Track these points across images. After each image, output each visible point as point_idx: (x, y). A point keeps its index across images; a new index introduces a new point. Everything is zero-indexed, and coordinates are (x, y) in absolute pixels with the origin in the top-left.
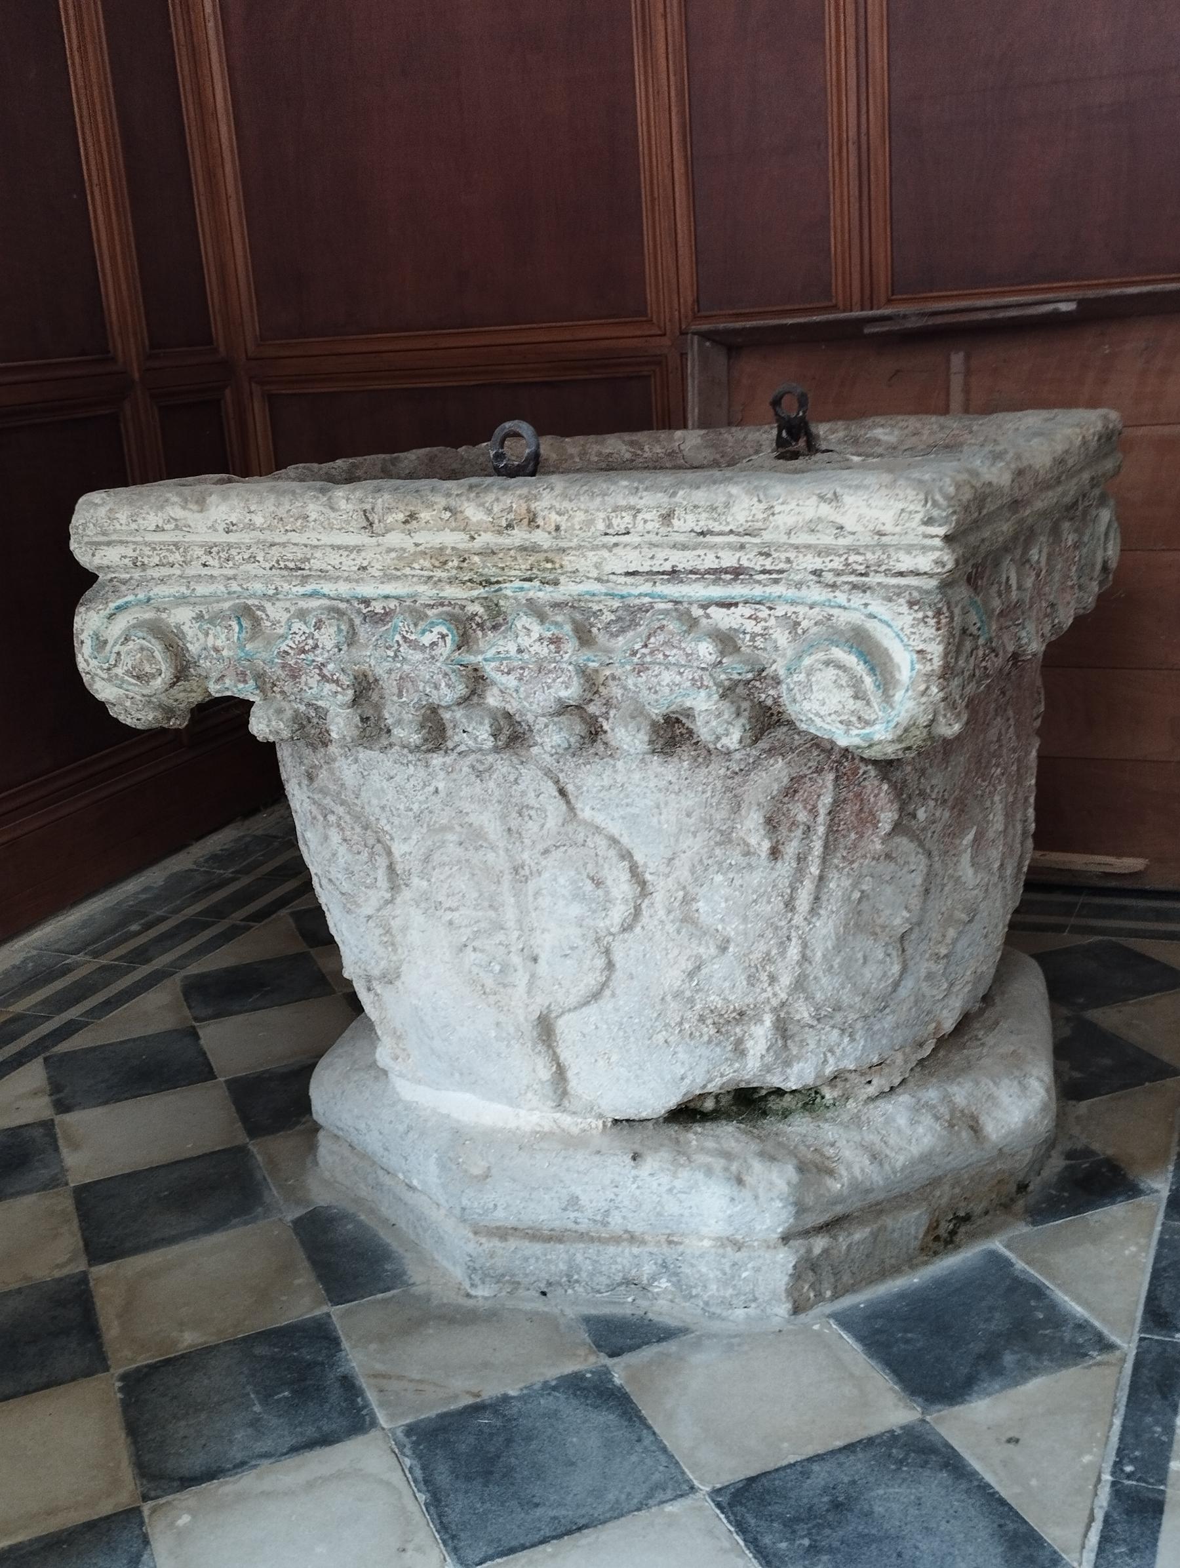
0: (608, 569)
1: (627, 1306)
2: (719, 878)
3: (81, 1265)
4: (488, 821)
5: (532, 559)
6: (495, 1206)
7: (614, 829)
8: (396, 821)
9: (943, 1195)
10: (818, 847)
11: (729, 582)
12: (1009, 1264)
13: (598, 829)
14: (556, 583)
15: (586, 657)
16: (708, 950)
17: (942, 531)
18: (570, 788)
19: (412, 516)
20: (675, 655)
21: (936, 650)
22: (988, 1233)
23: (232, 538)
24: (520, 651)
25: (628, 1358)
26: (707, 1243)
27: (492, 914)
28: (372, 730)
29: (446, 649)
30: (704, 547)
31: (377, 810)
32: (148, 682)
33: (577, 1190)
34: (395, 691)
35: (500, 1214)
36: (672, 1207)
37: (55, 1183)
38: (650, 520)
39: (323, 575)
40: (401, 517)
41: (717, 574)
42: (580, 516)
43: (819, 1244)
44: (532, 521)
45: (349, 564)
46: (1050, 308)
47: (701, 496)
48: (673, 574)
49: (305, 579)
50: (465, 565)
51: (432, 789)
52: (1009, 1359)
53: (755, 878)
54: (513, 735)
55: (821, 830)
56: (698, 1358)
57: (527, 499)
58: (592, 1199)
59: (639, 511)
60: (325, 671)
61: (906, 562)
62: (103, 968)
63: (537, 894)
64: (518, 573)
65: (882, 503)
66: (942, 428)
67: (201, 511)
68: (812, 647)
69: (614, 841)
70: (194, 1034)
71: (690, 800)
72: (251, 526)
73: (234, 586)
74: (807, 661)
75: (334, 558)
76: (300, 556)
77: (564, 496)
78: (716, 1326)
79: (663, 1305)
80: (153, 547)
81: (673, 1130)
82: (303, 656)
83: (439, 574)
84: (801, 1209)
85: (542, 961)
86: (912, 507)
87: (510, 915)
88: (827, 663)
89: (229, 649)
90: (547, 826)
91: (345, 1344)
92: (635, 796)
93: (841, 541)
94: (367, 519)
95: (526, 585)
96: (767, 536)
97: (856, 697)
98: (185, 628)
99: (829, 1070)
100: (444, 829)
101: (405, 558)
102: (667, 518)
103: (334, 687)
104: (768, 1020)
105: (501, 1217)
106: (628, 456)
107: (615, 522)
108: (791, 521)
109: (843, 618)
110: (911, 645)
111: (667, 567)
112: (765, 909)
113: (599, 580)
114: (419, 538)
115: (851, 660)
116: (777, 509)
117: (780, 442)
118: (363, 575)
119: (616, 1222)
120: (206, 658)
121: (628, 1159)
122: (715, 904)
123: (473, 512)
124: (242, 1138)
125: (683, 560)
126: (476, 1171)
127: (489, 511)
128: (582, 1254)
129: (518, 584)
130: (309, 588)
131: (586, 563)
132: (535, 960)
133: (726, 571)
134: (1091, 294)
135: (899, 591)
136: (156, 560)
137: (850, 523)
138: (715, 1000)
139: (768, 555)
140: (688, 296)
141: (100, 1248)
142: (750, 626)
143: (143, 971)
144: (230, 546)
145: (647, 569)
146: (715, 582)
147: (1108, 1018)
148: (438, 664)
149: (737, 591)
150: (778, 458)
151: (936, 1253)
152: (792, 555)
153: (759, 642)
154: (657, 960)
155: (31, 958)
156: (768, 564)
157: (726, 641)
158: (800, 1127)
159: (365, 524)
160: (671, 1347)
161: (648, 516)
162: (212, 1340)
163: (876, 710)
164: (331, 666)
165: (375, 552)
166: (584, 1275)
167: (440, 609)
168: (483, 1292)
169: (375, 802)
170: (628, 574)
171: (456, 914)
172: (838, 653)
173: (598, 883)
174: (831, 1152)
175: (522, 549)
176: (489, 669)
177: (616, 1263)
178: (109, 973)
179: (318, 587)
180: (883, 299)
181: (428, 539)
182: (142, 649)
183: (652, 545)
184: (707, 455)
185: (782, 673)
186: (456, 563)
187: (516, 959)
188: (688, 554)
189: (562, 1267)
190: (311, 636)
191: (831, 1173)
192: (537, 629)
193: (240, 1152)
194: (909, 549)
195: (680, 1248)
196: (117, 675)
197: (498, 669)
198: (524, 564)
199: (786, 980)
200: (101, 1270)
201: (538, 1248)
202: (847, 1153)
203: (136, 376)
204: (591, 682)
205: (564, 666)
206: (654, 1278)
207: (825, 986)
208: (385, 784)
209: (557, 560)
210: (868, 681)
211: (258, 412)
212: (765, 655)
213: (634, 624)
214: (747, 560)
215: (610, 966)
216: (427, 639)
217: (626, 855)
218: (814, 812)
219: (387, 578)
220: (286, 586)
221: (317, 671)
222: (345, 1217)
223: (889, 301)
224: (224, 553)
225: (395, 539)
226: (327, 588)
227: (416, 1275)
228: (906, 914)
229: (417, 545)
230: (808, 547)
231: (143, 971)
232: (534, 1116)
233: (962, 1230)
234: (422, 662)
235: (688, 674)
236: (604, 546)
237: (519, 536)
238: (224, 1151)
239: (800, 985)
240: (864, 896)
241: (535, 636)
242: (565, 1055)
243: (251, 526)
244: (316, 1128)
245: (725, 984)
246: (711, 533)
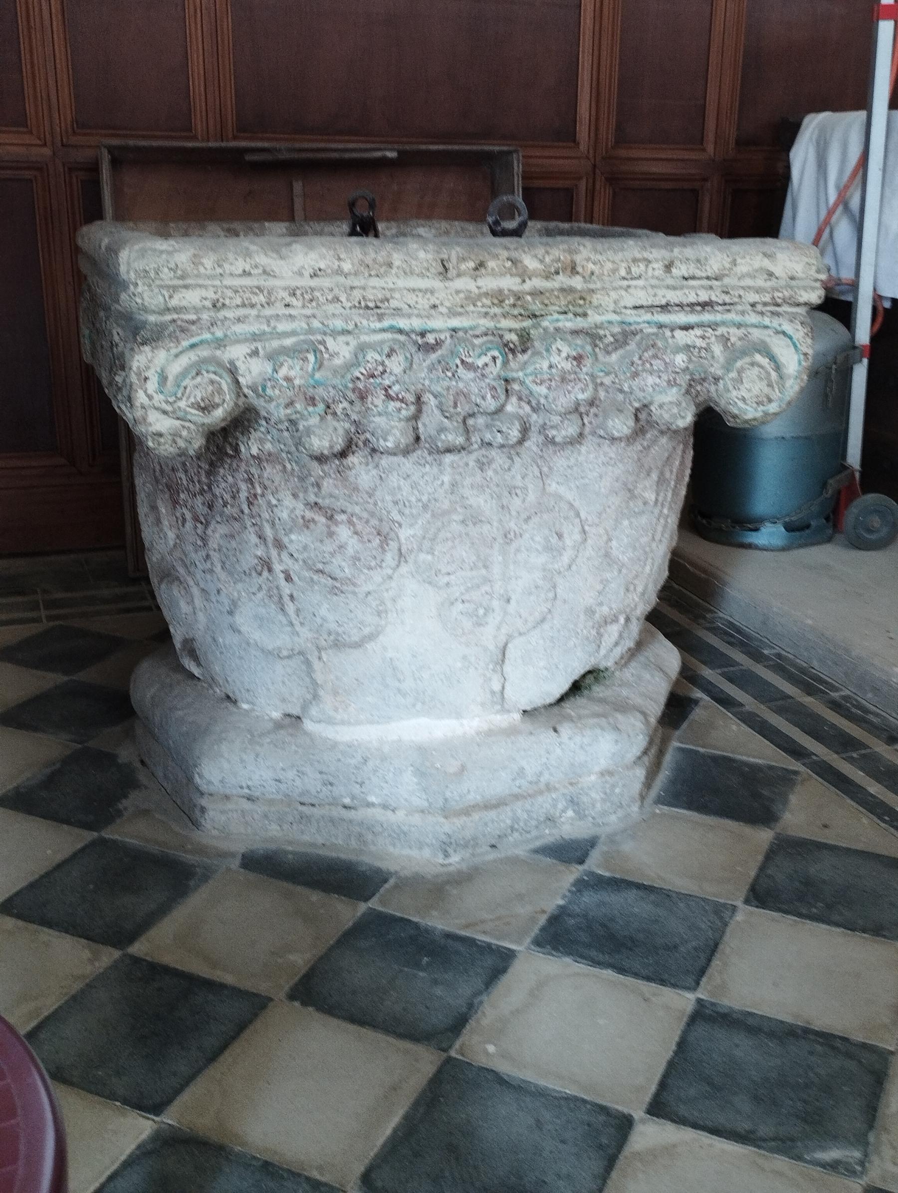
0: (622, 304)
4: (482, 502)
5: (570, 298)
6: (469, 791)
8: (407, 511)
11: (699, 312)
12: (697, 752)
14: (585, 315)
23: (314, 283)
24: (551, 367)
26: (593, 778)
27: (484, 571)
31: (390, 505)
32: (209, 412)
33: (524, 763)
34: (452, 404)
35: (471, 797)
40: (471, 265)
42: (609, 266)
45: (424, 303)
46: (378, 154)
47: (689, 252)
48: (665, 308)
49: (380, 317)
50: (519, 303)
51: (439, 482)
57: (570, 252)
58: (531, 768)
59: (650, 262)
60: (390, 392)
63: (518, 550)
64: (557, 308)
65: (797, 259)
68: (744, 353)
72: (339, 272)
73: (316, 324)
74: (739, 364)
75: (411, 299)
76: (380, 296)
81: (556, 710)
82: (372, 380)
83: (496, 310)
85: (513, 602)
87: (496, 570)
88: (753, 364)
89: (301, 377)
90: (529, 499)
94: (444, 266)
95: (562, 317)
97: (768, 385)
98: (239, 364)
100: (445, 513)
101: (472, 299)
102: (668, 267)
103: (398, 404)
105: (473, 797)
107: (633, 269)
111: (663, 302)
113: (615, 312)
114: (480, 282)
116: (739, 261)
118: (433, 312)
120: (273, 387)
125: (674, 297)
126: (452, 770)
127: (542, 261)
128: (519, 809)
129: (556, 316)
130: (386, 323)
132: (508, 601)
133: (699, 304)
134: (407, 147)
136: (238, 301)
137: (778, 270)
139: (727, 293)
144: (312, 290)
145: (650, 303)
146: (692, 311)
148: (487, 381)
149: (707, 317)
152: (742, 293)
156: (727, 299)
159: (441, 269)
161: (656, 266)
164: (396, 388)
165: (446, 292)
166: (522, 824)
167: (485, 338)
168: (455, 859)
169: (388, 498)
170: (636, 308)
171: (452, 577)
175: (562, 290)
177: (542, 807)
179: (394, 323)
180: (230, 136)
181: (488, 283)
182: (212, 382)
186: (512, 301)
187: (495, 604)
188: (679, 293)
189: (509, 822)
190: (383, 364)
192: (566, 350)
194: (805, 288)
195: (579, 786)
196: (179, 408)
197: (534, 382)
201: (492, 814)
205: (582, 376)
208: (402, 482)
209: (588, 298)
212: (706, 362)
214: (716, 296)
216: (480, 363)
219: (452, 313)
220: (365, 322)
221: (383, 392)
223: (235, 138)
224: (310, 297)
225: (465, 284)
226: (403, 323)
229: (478, 288)
230: (749, 287)
234: (474, 380)
235: (665, 377)
236: (621, 288)
237: (562, 280)
241: (564, 355)
243: (339, 272)
246: (693, 278)
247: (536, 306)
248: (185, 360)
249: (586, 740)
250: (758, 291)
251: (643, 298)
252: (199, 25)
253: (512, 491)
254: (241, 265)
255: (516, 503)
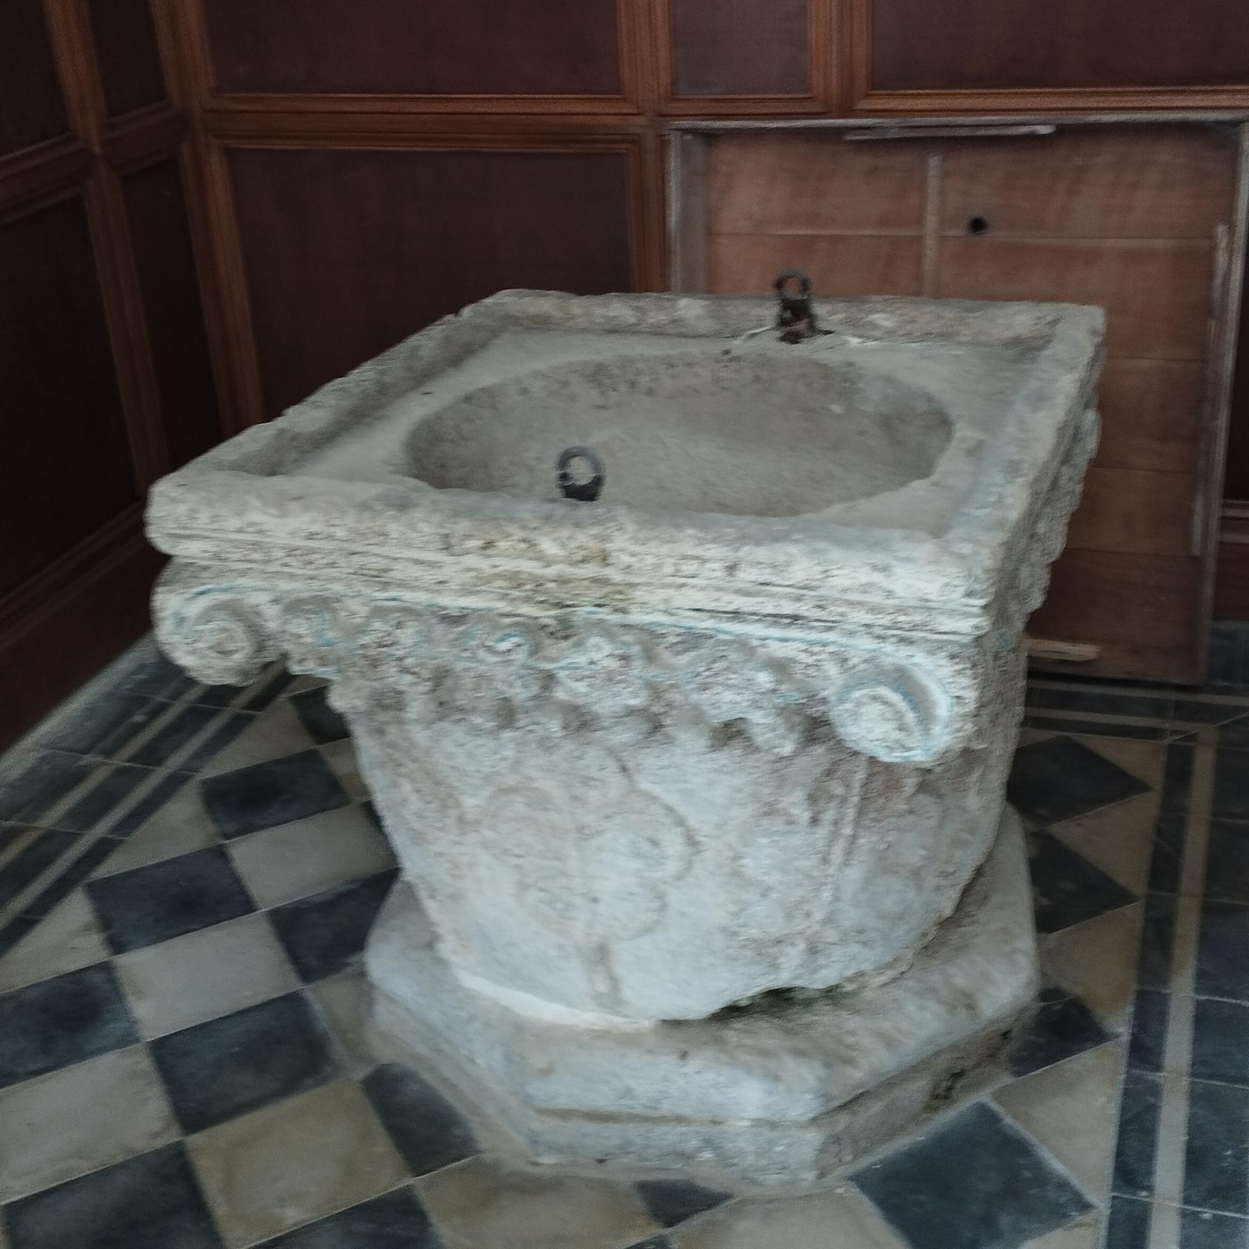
0: (675, 604)
1: (675, 1173)
2: (764, 841)
3: (173, 1136)
5: (605, 590)
7: (670, 799)
9: (942, 1064)
10: (851, 813)
13: (654, 799)
15: (652, 672)
16: (749, 895)
17: (982, 602)
18: (630, 765)
19: (489, 545)
20: (735, 679)
21: (971, 695)
22: (978, 1085)
25: (682, 1227)
28: (444, 708)
29: (520, 656)
30: (768, 596)
33: (631, 1083)
36: (716, 1098)
37: (128, 1039)
38: (715, 570)
39: (402, 584)
40: (480, 543)
41: (776, 619)
42: (650, 560)
43: (843, 1121)
44: (604, 558)
48: (736, 615)
49: (386, 585)
52: (1005, 1220)
53: (796, 841)
54: (581, 721)
55: (856, 800)
56: (743, 1226)
61: (948, 624)
62: (120, 772)
66: (940, 317)
67: (280, 517)
68: (860, 683)
69: (670, 810)
70: (221, 854)
71: (740, 780)
74: (857, 694)
75: (415, 571)
77: (635, 540)
78: (755, 1191)
79: (705, 1172)
80: (236, 544)
81: (714, 1028)
83: (515, 593)
84: (826, 1097)
86: (956, 582)
88: (875, 698)
91: (434, 1218)
92: (691, 777)
93: (891, 602)
96: (822, 592)
97: (901, 729)
99: (850, 972)
102: (732, 569)
104: (802, 946)
105: (563, 1102)
106: (632, 320)
108: (846, 583)
109: (887, 661)
110: (951, 692)
111: (731, 608)
112: (803, 863)
115: (895, 698)
117: (783, 322)
119: (666, 1108)
121: (674, 1058)
122: (760, 859)
123: (549, 546)
124: (295, 985)
127: (564, 546)
128: (633, 1132)
131: (657, 597)
133: (787, 616)
135: (941, 646)
138: (754, 932)
140: (665, 78)
141: (194, 1115)
142: (804, 658)
143: (158, 776)
144: (313, 551)
147: (1069, 832)
150: (783, 339)
151: (937, 1109)
153: (811, 671)
154: (705, 902)
155: (44, 758)
157: (780, 667)
158: (824, 1019)
160: (716, 1213)
162: (314, 1217)
163: (915, 740)
165: (453, 568)
168: (547, 1160)
172: (884, 691)
173: (655, 843)
174: (850, 1040)
175: (595, 580)
176: (562, 674)
178: (127, 777)
183: (718, 589)
184: (708, 325)
185: (833, 699)
189: (617, 1142)
191: (849, 1061)
192: (608, 648)
193: (294, 1000)
194: (951, 613)
198: (597, 593)
199: (819, 915)
200: (196, 1140)
202: (867, 1041)
203: (98, 150)
204: (656, 691)
206: (699, 1150)
207: (851, 916)
210: (910, 717)
211: (216, 168)
213: (695, 647)
214: (803, 609)
215: (663, 908)
217: (681, 822)
218: (848, 786)
219: (467, 591)
222: (409, 1076)
225: (472, 561)
227: (483, 1139)
228: (923, 852)
231: (158, 776)
232: (588, 1017)
233: (958, 1085)
238: (279, 999)
239: (829, 920)
240: (890, 845)
242: (619, 970)
243: (330, 537)
244: (372, 986)
245: (765, 918)
247: (562, 594)
248: (203, 603)
249: (722, 1079)
250: (874, 609)
251: (699, 599)
252: (443, 136)
253: (587, 781)
254: (234, 523)
255: (594, 795)
